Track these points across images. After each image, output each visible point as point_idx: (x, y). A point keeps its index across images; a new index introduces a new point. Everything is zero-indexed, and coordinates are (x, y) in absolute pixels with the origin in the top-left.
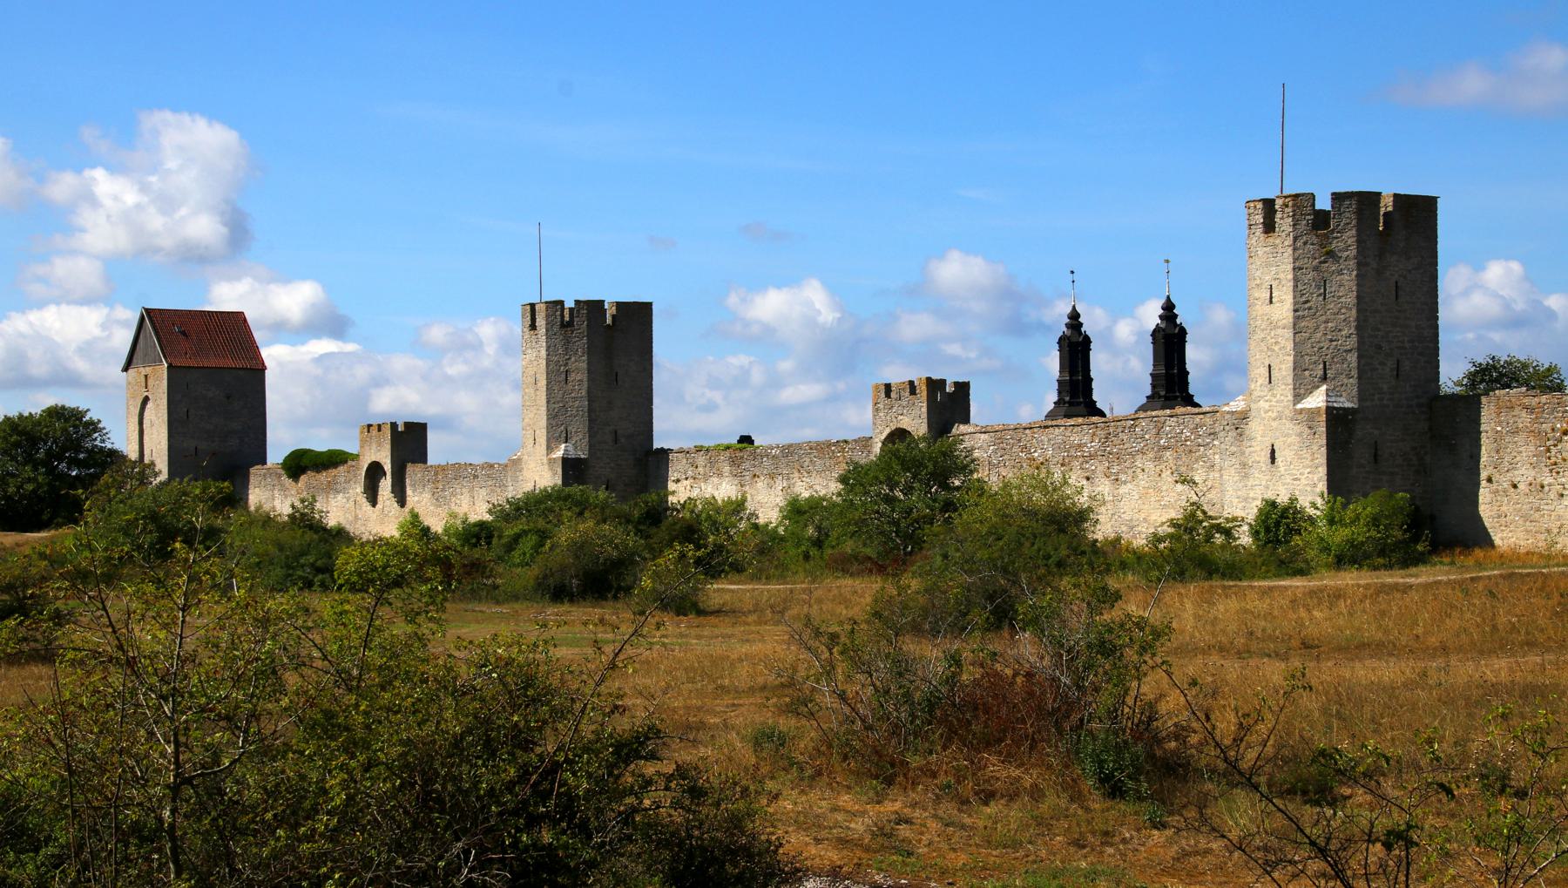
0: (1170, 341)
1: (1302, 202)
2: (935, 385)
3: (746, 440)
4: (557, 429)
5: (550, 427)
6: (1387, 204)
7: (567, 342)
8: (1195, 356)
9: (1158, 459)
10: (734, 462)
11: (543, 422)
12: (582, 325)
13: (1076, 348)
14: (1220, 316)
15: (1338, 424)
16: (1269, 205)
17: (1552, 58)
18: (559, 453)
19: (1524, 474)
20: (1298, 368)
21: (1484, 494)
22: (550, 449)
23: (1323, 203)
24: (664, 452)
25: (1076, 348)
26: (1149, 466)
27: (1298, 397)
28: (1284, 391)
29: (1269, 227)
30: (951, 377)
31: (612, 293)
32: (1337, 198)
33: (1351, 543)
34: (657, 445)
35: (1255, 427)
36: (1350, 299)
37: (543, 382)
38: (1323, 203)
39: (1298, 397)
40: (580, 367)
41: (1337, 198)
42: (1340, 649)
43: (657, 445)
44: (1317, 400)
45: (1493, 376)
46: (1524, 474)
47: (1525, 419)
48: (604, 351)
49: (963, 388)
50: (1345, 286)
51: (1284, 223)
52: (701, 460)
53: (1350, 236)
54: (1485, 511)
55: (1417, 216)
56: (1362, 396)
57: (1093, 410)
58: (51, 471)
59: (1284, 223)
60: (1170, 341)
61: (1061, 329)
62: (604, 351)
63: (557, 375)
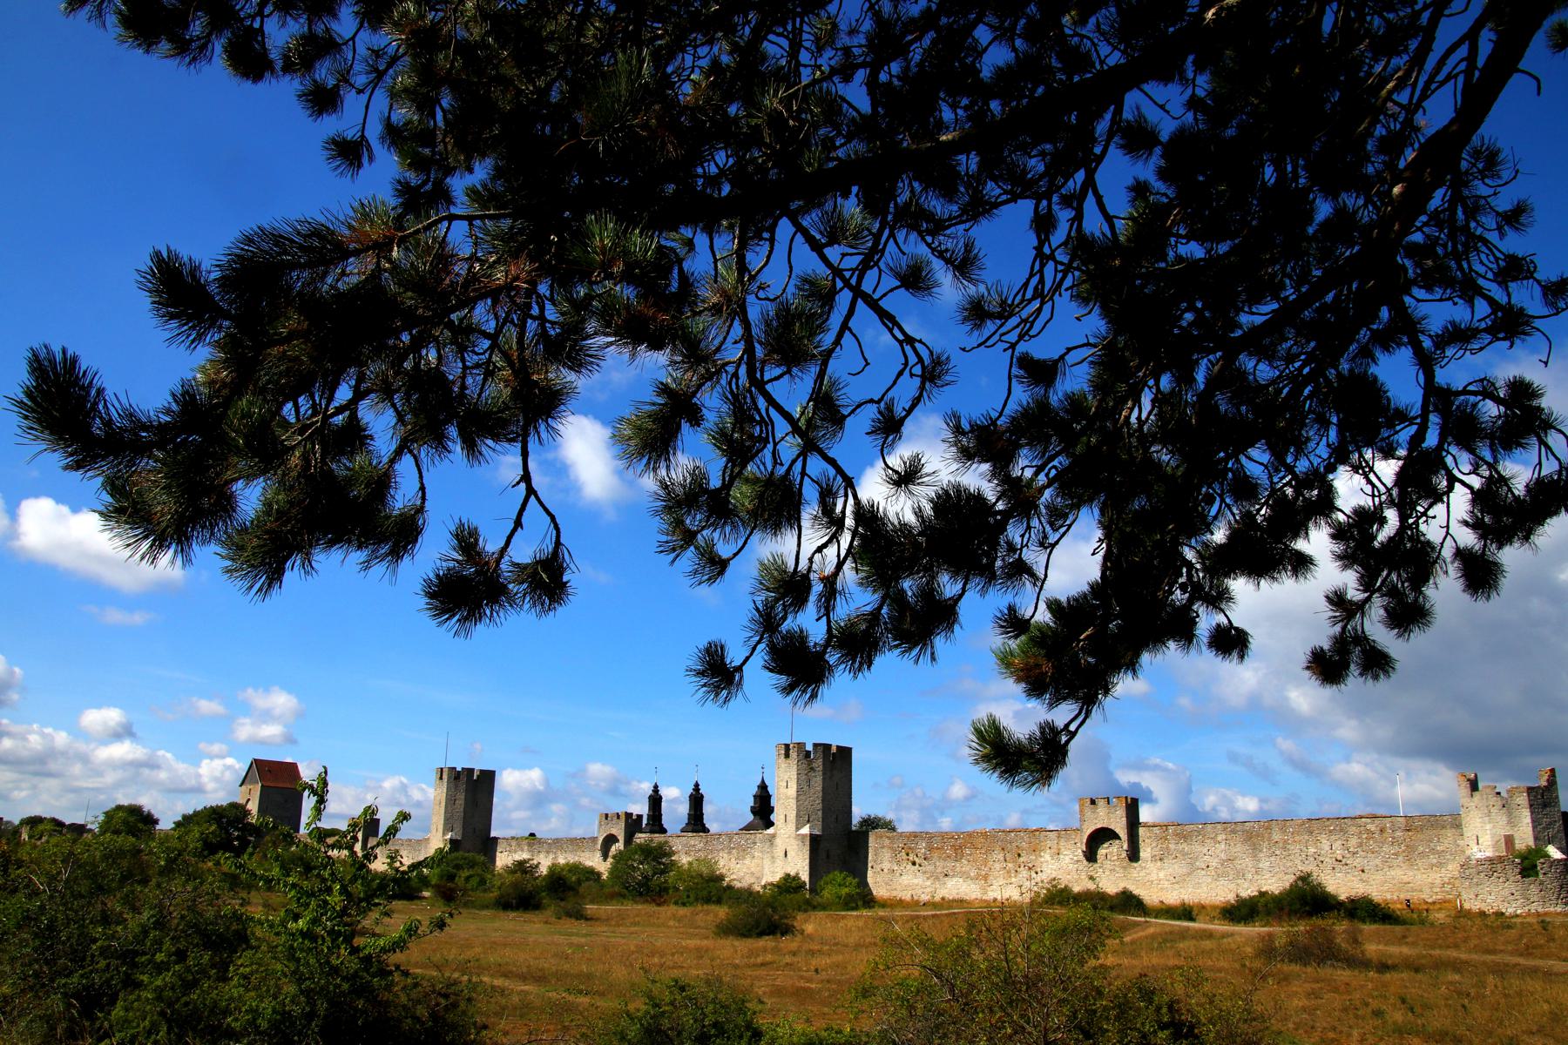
0: (697, 800)
1: (801, 745)
2: (628, 815)
3: (532, 835)
4: (448, 827)
6: (834, 750)
7: (456, 787)
8: (708, 809)
10: (529, 845)
12: (464, 779)
15: (814, 841)
16: (787, 746)
18: (448, 837)
19: (886, 865)
20: (798, 816)
21: (870, 873)
23: (809, 748)
24: (496, 839)
27: (798, 829)
28: (792, 825)
29: (787, 755)
31: (479, 766)
32: (815, 745)
33: (848, 895)
34: (493, 834)
35: (778, 841)
36: (819, 788)
38: (809, 748)
39: (798, 829)
40: (461, 797)
41: (815, 745)
43: (493, 834)
44: (806, 830)
45: (871, 823)
46: (886, 865)
47: (887, 842)
48: (473, 790)
50: (818, 781)
51: (793, 754)
52: (514, 843)
53: (820, 762)
54: (870, 880)
55: (845, 753)
56: (823, 829)
57: (706, 830)
58: (227, 832)
59: (793, 754)
60: (697, 800)
61: (755, 790)
63: (451, 801)
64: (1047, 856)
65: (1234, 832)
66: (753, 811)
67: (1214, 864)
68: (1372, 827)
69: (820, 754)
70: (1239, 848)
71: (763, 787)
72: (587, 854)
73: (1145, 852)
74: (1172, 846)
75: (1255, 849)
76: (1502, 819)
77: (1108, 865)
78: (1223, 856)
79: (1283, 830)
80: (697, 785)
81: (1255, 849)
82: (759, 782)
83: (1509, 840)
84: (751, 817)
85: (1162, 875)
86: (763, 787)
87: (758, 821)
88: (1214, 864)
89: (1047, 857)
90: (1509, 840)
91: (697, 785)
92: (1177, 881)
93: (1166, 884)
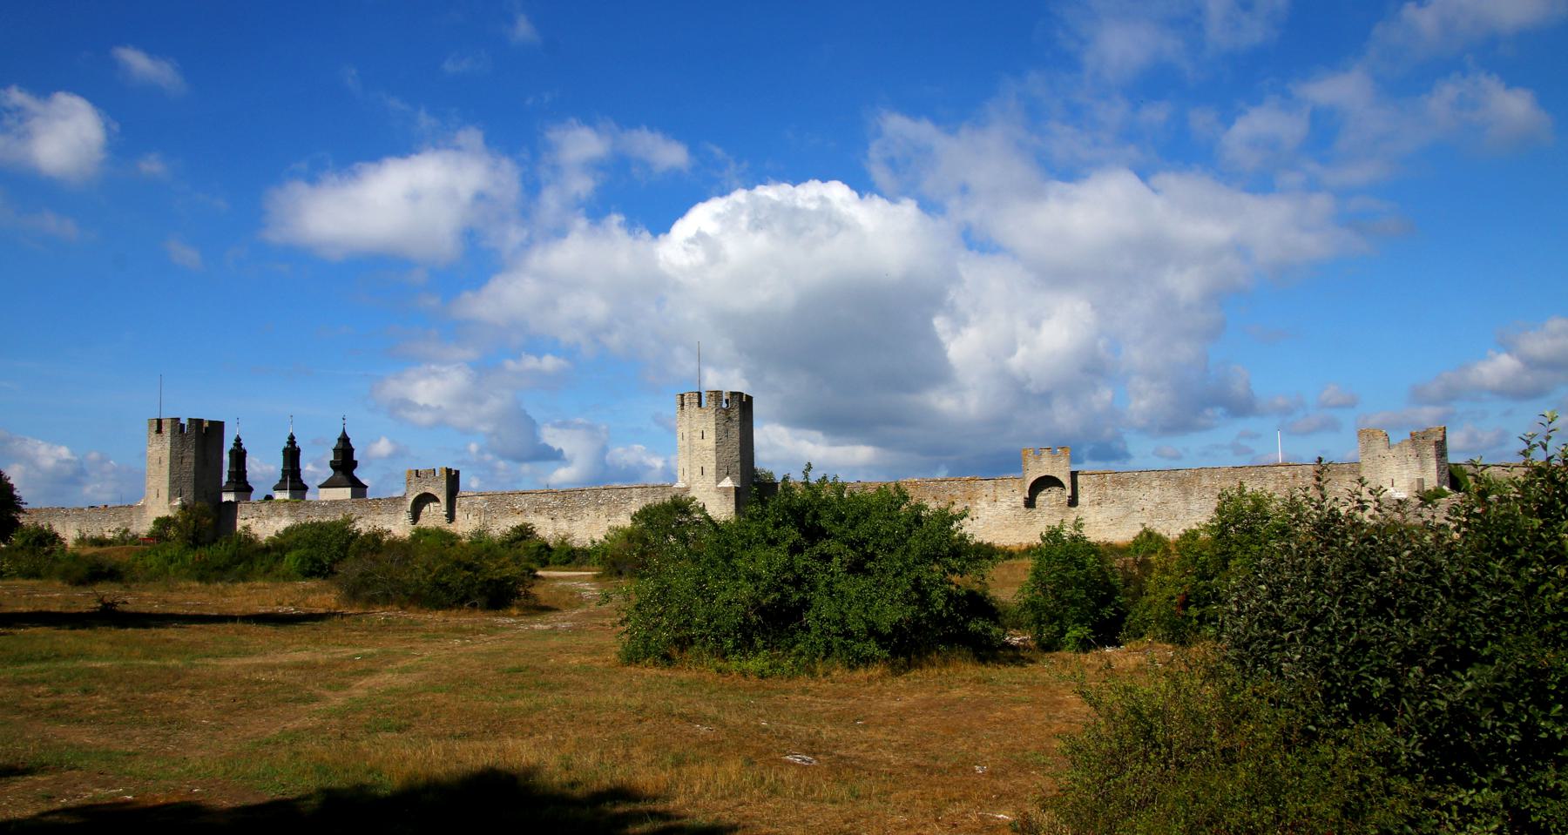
4: (175, 489)
5: (171, 488)
7: (183, 441)
9: (597, 509)
10: (291, 509)
11: (167, 485)
13: (292, 455)
14: (383, 447)
17: (1555, 324)
20: (718, 469)
22: (170, 500)
25: (292, 455)
26: (592, 513)
27: (718, 482)
30: (454, 468)
36: (737, 439)
37: (166, 463)
41: (733, 394)
42: (217, 568)
44: (728, 483)
49: (457, 472)
51: (166, 429)
59: (166, 429)
61: (334, 443)
62: (203, 448)
63: (176, 459)
64: (983, 504)
65: (1167, 478)
66: (333, 465)
67: (1149, 506)
68: (1286, 474)
69: (736, 403)
70: (1171, 493)
71: (344, 439)
72: (386, 517)
73: (1083, 498)
74: (1109, 492)
75: (1186, 493)
76: (1415, 465)
77: (1047, 510)
78: (1157, 500)
79: (1211, 477)
80: (292, 439)
81: (1186, 493)
82: (339, 434)
83: (1421, 481)
84: (331, 472)
85: (1099, 518)
86: (344, 439)
87: (340, 476)
88: (1149, 506)
89: (984, 504)
90: (1421, 481)
91: (292, 439)
92: (1115, 523)
93: (1104, 526)
